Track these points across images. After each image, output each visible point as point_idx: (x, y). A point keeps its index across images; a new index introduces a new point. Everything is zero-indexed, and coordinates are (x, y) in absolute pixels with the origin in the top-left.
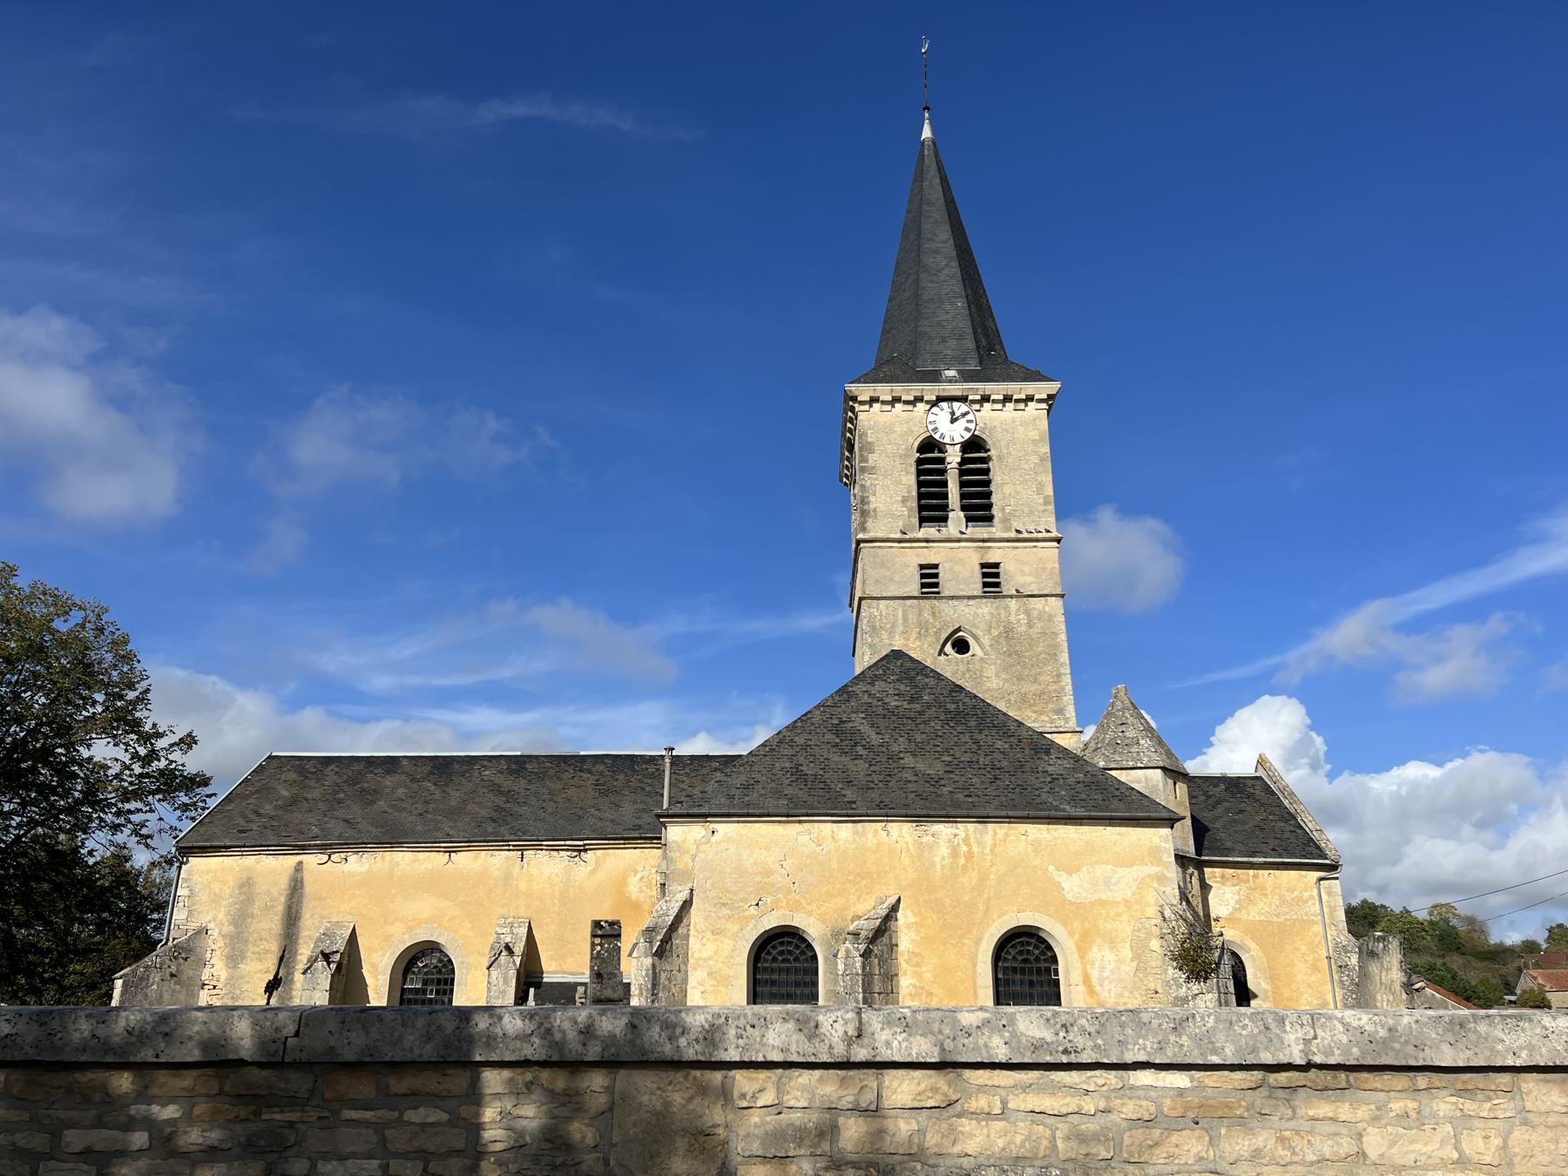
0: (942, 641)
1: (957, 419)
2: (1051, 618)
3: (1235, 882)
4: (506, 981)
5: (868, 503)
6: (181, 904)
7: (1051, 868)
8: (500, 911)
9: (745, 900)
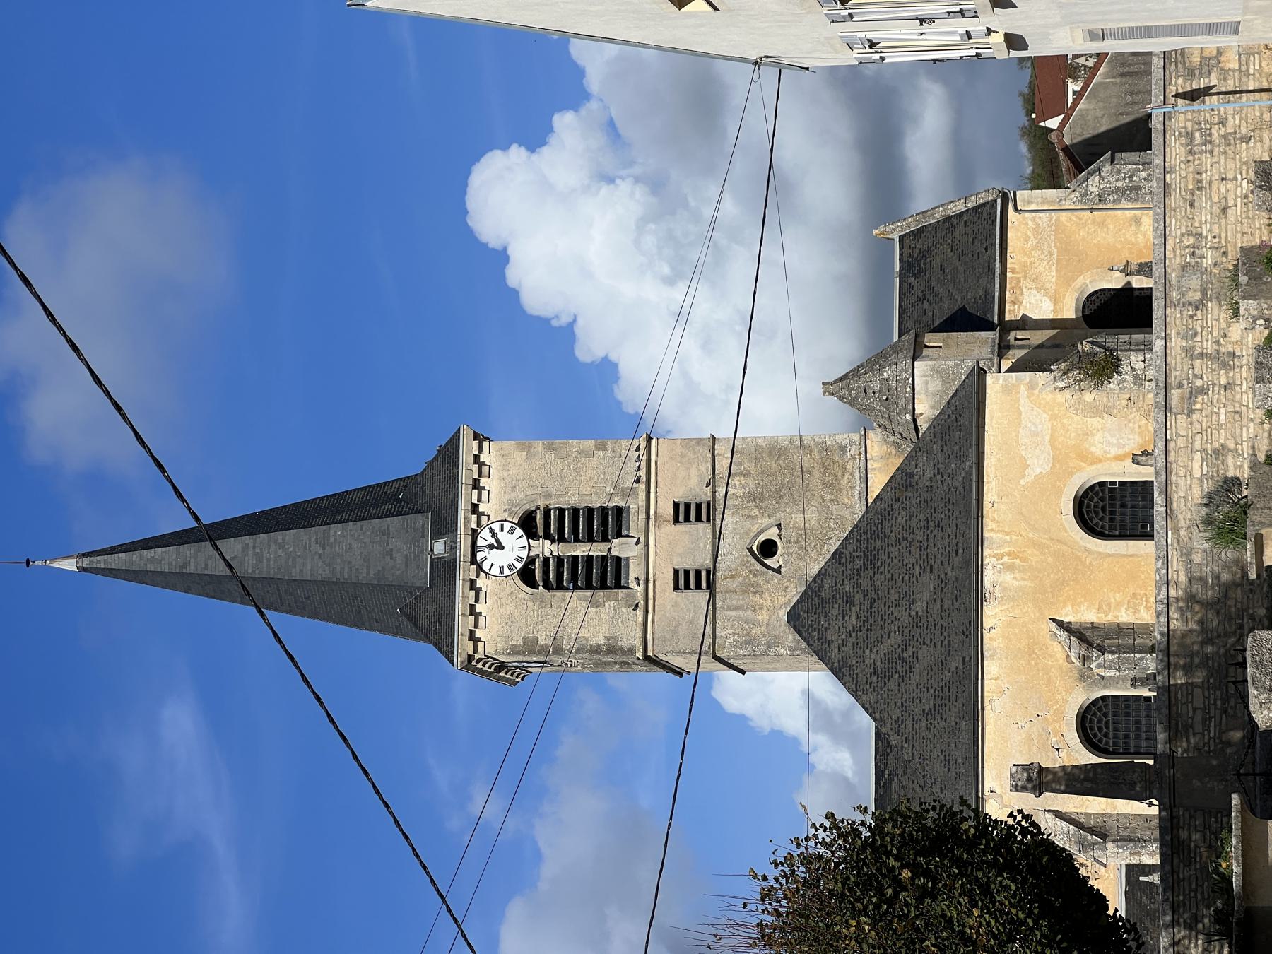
1: (498, 541)
3: (1019, 292)
5: (599, 645)
7: (1022, 482)
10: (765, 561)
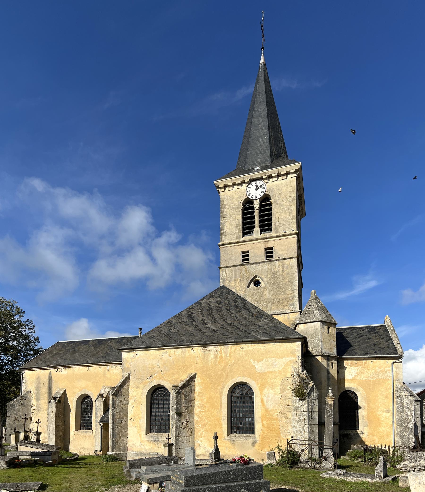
0: (249, 282)
4: (100, 405)
5: (223, 230)
6: (24, 385)
7: (251, 360)
8: (103, 384)
9: (146, 377)
10: (252, 283)
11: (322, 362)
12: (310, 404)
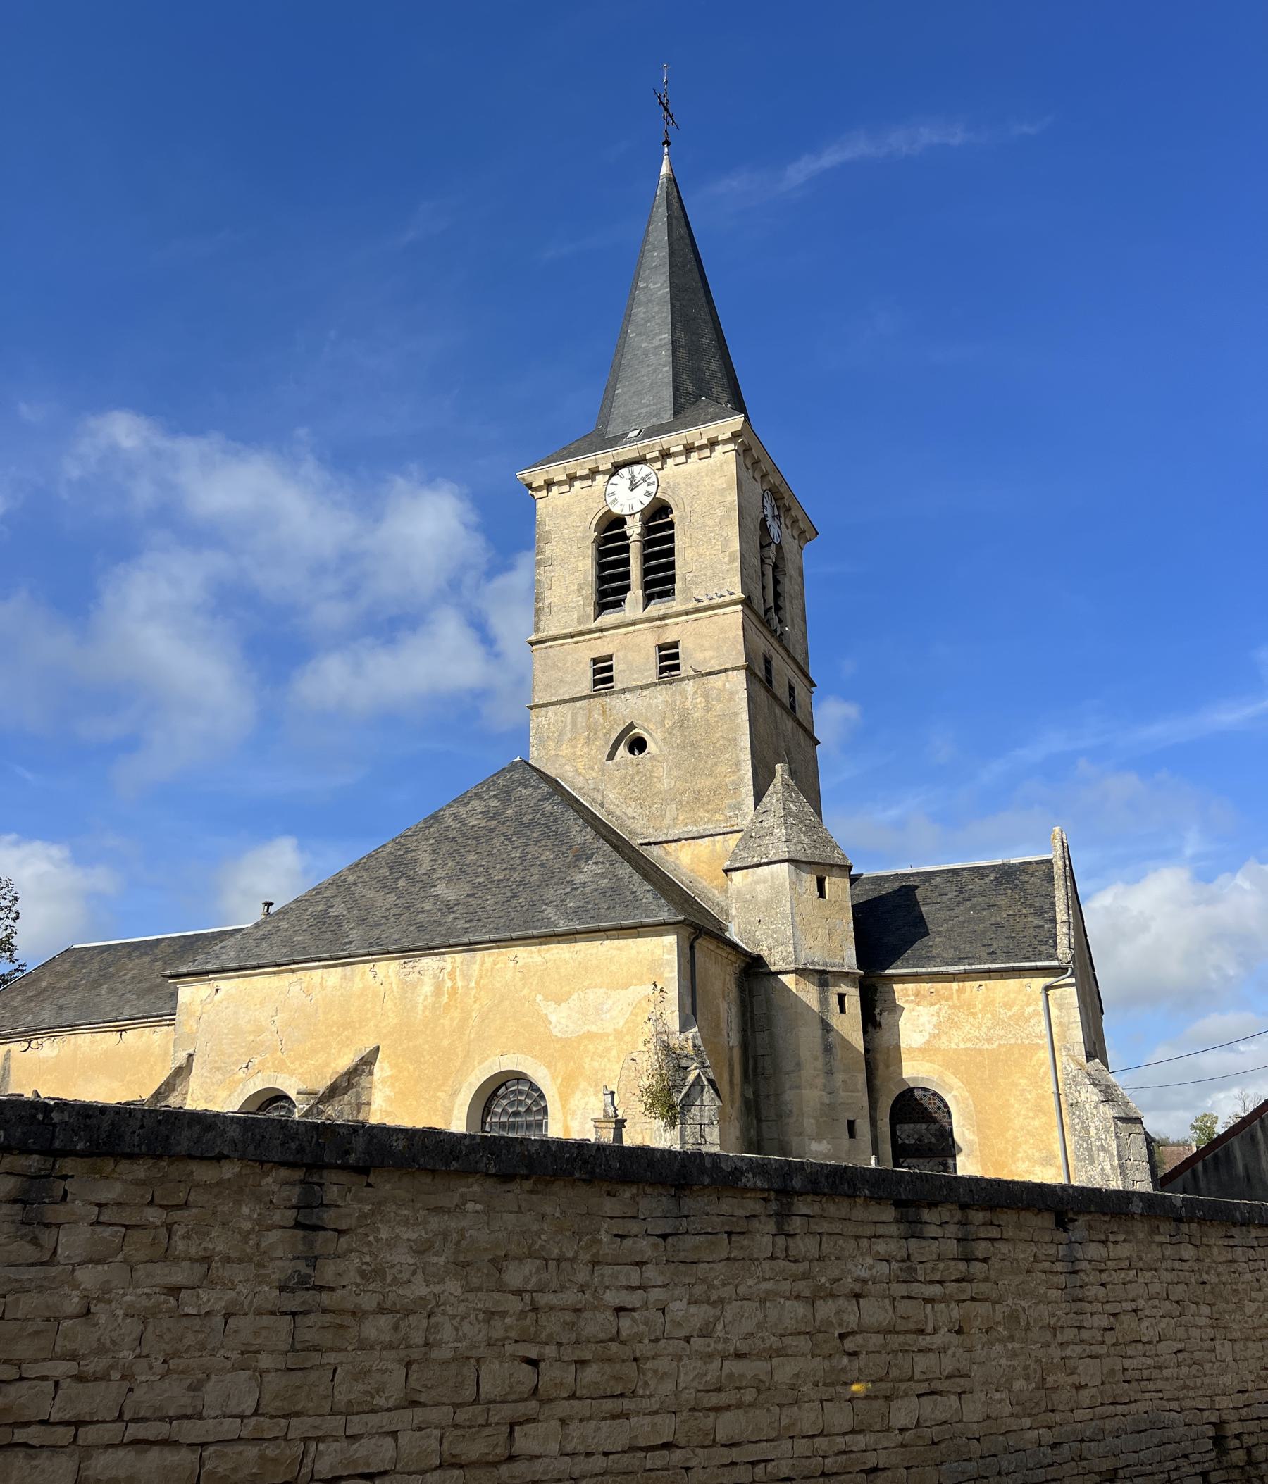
2: (731, 695)
5: (543, 599)
7: (539, 998)
9: (236, 1063)
11: (800, 994)
12: (691, 1141)
